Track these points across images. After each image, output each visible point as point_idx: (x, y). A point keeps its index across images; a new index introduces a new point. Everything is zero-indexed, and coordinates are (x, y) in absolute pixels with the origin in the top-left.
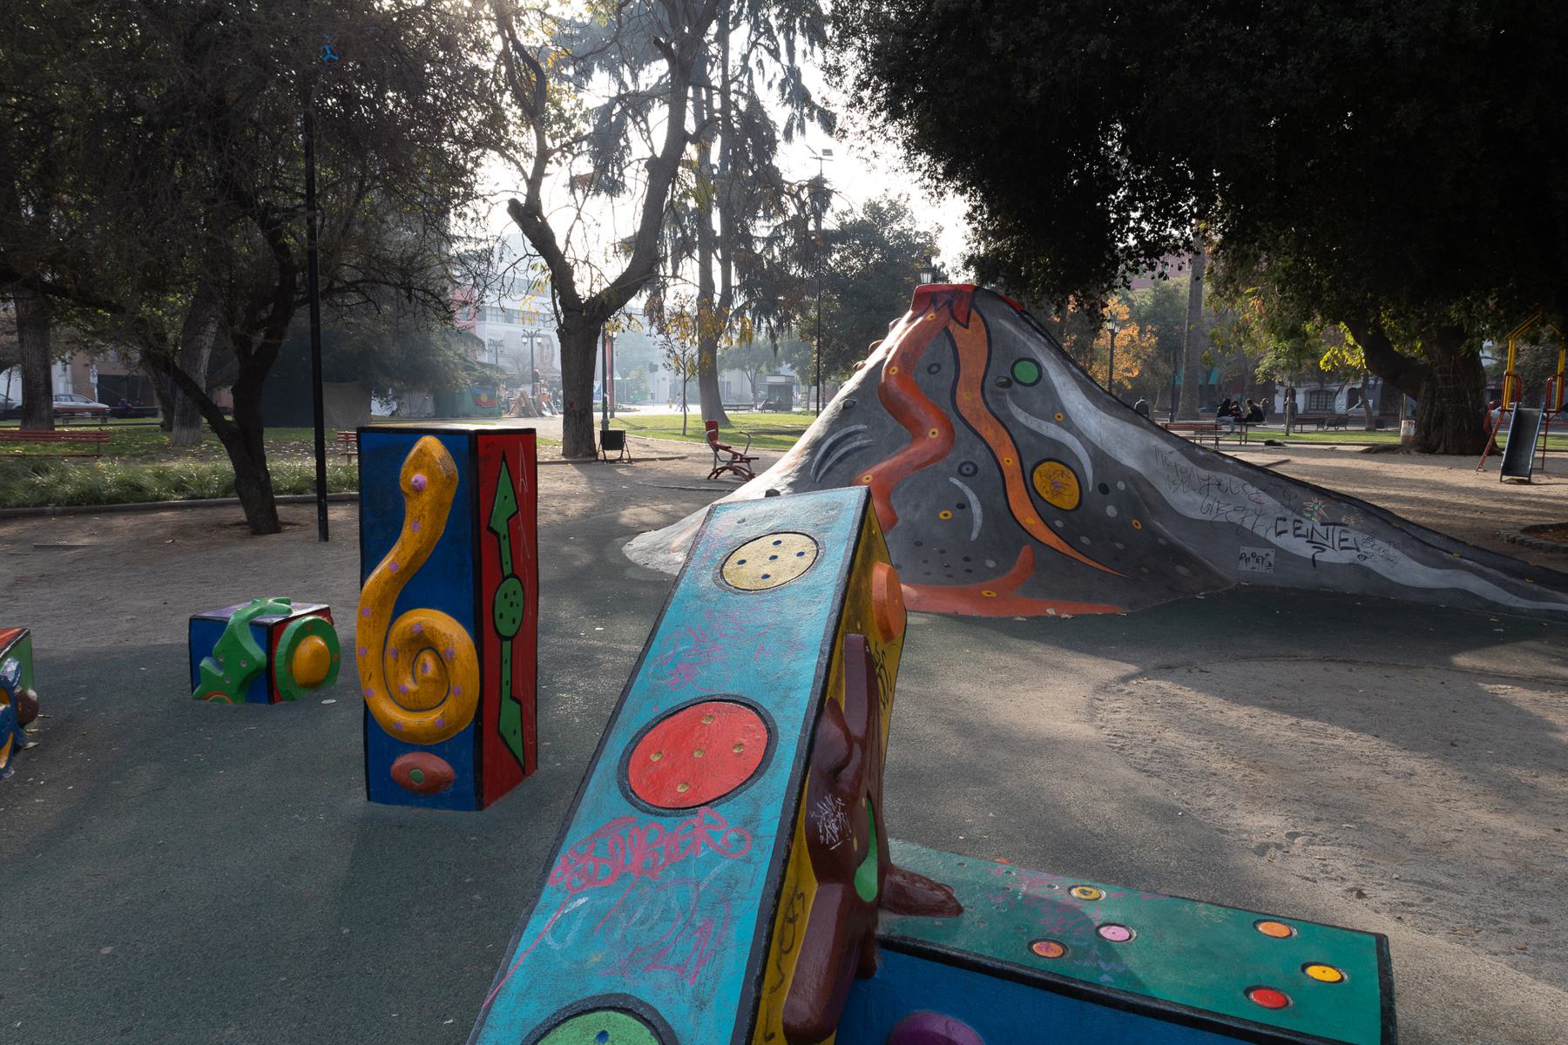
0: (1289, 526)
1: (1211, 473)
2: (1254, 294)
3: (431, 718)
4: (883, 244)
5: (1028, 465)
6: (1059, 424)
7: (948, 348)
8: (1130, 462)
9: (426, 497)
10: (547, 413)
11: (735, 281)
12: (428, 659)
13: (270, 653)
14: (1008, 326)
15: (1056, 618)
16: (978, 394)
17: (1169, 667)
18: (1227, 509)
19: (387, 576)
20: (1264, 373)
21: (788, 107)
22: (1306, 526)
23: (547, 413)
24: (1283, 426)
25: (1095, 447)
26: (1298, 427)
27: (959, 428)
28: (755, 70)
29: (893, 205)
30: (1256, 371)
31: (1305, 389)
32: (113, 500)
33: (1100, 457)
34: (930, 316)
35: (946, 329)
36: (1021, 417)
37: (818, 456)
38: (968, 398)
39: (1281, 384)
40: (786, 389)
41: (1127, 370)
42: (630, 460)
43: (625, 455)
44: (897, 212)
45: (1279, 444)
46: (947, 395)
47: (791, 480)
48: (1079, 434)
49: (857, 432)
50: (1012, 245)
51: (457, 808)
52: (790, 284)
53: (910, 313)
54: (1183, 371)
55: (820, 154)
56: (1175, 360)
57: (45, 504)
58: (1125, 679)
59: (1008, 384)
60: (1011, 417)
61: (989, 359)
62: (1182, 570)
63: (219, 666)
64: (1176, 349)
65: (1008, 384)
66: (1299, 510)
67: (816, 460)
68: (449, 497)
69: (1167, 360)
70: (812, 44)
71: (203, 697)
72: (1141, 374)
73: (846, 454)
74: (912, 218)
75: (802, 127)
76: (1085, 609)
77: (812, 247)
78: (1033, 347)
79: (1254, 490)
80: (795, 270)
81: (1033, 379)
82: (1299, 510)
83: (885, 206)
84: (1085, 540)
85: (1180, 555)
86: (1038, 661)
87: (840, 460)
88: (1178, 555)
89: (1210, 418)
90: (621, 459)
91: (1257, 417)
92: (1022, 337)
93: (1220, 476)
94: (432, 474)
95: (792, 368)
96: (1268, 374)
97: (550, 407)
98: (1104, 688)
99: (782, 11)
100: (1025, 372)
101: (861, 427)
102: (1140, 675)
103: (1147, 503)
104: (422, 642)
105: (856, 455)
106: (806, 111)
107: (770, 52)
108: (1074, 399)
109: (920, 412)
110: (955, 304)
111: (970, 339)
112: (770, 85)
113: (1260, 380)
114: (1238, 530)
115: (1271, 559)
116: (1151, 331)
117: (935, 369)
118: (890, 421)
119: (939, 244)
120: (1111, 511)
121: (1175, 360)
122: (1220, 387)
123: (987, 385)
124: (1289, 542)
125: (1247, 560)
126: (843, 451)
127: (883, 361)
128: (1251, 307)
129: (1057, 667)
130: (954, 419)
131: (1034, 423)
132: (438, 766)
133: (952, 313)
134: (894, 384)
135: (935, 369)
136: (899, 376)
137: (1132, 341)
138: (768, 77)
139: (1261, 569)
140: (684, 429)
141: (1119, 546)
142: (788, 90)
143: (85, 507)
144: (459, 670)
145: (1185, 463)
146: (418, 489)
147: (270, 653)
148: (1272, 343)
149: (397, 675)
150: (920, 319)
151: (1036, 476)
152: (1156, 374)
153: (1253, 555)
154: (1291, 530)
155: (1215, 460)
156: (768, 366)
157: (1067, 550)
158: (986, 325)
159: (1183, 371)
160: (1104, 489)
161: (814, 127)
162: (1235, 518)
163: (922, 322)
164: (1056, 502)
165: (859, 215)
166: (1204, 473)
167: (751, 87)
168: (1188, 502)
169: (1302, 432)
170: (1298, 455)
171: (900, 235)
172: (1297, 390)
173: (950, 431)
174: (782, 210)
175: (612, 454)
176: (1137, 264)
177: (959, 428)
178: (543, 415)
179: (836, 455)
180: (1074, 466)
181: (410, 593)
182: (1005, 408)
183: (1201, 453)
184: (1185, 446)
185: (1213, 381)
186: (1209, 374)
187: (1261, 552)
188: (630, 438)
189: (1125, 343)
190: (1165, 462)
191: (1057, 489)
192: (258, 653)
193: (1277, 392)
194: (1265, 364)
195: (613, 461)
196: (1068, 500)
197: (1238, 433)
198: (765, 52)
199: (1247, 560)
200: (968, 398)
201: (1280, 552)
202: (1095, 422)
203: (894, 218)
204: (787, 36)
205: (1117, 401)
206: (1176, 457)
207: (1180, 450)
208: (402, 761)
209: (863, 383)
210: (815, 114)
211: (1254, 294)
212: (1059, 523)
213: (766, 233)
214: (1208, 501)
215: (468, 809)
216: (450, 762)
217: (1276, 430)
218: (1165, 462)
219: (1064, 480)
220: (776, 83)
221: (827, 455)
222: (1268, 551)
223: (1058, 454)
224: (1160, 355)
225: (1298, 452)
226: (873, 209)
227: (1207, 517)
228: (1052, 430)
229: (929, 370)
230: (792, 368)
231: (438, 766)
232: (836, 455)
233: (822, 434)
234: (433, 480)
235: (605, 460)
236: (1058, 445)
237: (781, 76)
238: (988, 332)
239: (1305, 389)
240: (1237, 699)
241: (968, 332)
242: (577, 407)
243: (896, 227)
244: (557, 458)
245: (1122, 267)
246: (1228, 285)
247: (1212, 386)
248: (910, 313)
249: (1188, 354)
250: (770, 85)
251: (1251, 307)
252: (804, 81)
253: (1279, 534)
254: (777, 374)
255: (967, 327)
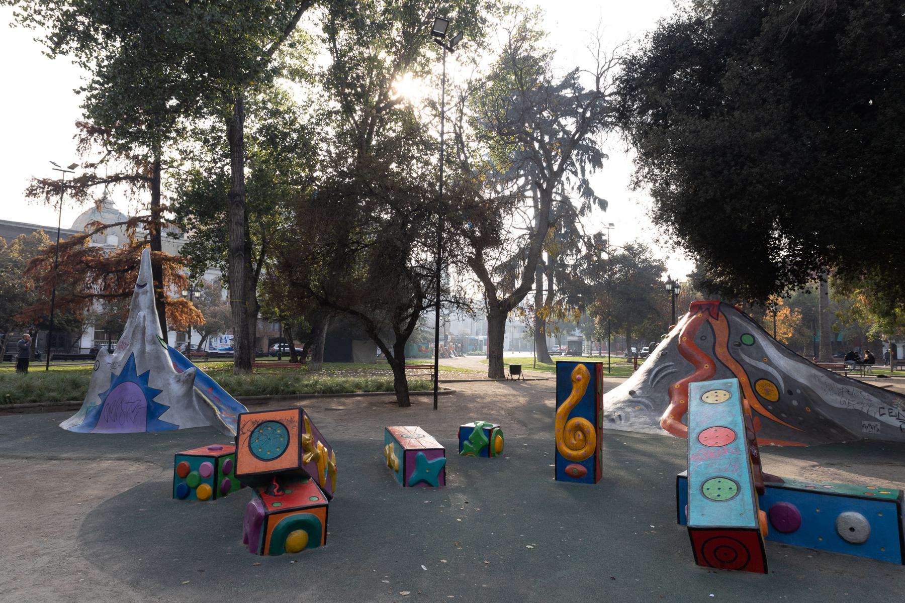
0: (886, 411)
1: (844, 386)
2: (859, 293)
3: (581, 452)
4: (635, 266)
5: (753, 381)
6: (765, 363)
7: (710, 330)
8: (802, 380)
9: (581, 382)
10: (453, 356)
11: (555, 287)
12: (580, 433)
13: (490, 440)
14: (738, 319)
15: (776, 447)
16: (726, 349)
17: (832, 464)
18: (853, 403)
19: (568, 406)
20: (872, 336)
21: (583, 198)
22: (895, 412)
23: (453, 356)
24: (889, 367)
25: (784, 373)
26: (899, 368)
27: (718, 364)
28: (565, 182)
29: (640, 245)
30: (868, 334)
31: (902, 344)
32: (337, 392)
33: (787, 378)
34: (699, 315)
35: (708, 321)
36: (747, 359)
37: (652, 376)
38: (721, 351)
39: (886, 341)
40: (579, 343)
41: (785, 333)
42: (524, 380)
43: (521, 378)
44: (643, 250)
45: (886, 377)
46: (711, 350)
47: (640, 386)
48: (776, 368)
49: (670, 366)
50: (729, 279)
51: (587, 483)
52: (587, 290)
53: (689, 313)
54: (820, 334)
55: (608, 226)
56: (814, 327)
57: (314, 393)
58: (814, 466)
59: (739, 345)
60: (743, 360)
61: (729, 334)
62: (833, 431)
63: (471, 443)
64: (815, 320)
65: (739, 345)
66: (891, 404)
67: (197, 408)
68: (588, 383)
69: (809, 328)
70: (594, 167)
71: (464, 454)
72: (793, 335)
73: (665, 375)
74: (651, 252)
75: (589, 207)
76: (789, 444)
77: (597, 268)
78: (750, 329)
79: (867, 394)
80: (587, 281)
81: (751, 343)
82: (891, 404)
83: (636, 246)
84: (784, 415)
85: (831, 424)
86: (773, 460)
87: (662, 378)
88: (831, 424)
89: (840, 361)
90: (519, 379)
91: (871, 361)
92: (744, 324)
93: (848, 387)
94: (583, 375)
95: (582, 332)
96: (877, 335)
97: (454, 353)
98: (805, 468)
99: (578, 152)
100: (747, 340)
101: (671, 363)
102: (820, 465)
103: (812, 400)
104: (579, 428)
105: (670, 376)
106: (592, 200)
107: (573, 173)
108: (772, 352)
109: (699, 358)
110: (711, 309)
111: (719, 325)
112: (573, 188)
113: (870, 340)
114: (860, 413)
115: (879, 427)
116: (798, 311)
117: (704, 338)
118: (685, 362)
119: (667, 266)
120: (795, 403)
121: (814, 327)
122: (845, 343)
123: (729, 345)
124: (886, 419)
125: (866, 427)
126: (663, 374)
127: (678, 334)
128: (859, 299)
129: (782, 462)
130: (715, 360)
131: (753, 362)
132: (581, 468)
133: (710, 314)
134: (685, 345)
135: (704, 338)
136: (687, 341)
137: (786, 316)
138: (572, 184)
139: (874, 432)
140: (535, 365)
141: (801, 419)
142: (582, 190)
143: (328, 394)
144: (591, 436)
145: (830, 381)
146: (579, 380)
147: (490, 440)
148: (876, 318)
149: (570, 438)
150: (694, 316)
151: (757, 386)
152: (803, 336)
153: (869, 425)
154: (887, 414)
155: (845, 380)
156: (567, 331)
157: (775, 419)
158: (727, 319)
159: (820, 334)
160: (790, 392)
161: (595, 207)
162: (858, 407)
163: (695, 319)
164: (767, 398)
165: (620, 252)
166: (840, 386)
167: (563, 190)
168: (834, 399)
169: (902, 370)
170: (897, 383)
171: (644, 261)
172: (897, 344)
173: (714, 366)
174: (579, 251)
175: (516, 377)
176: (793, 286)
177: (718, 364)
178: (451, 357)
179: (661, 376)
180: (775, 382)
181: (573, 412)
182: (739, 355)
183: (838, 377)
184: (831, 375)
185: (840, 339)
186: (837, 335)
187: (873, 424)
188: (523, 371)
189: (782, 318)
190: (820, 381)
191: (768, 392)
192: (486, 439)
193: (883, 346)
194: (873, 330)
195: (515, 380)
196: (774, 397)
197: (858, 370)
198: (570, 173)
199: (866, 427)
200: (721, 351)
201: (882, 423)
202: (783, 362)
203: (640, 252)
204: (581, 164)
205: (790, 349)
206: (825, 378)
207: (827, 375)
208: (568, 468)
209: (670, 344)
210: (597, 200)
211: (859, 293)
212: (770, 407)
213: (572, 262)
214: (843, 399)
215: (591, 483)
216: (585, 467)
217: (885, 369)
218: (820, 381)
219: (770, 388)
220: (576, 188)
221: (656, 375)
222: (877, 423)
223: (766, 376)
224: (804, 324)
225: (898, 382)
226: (629, 248)
227: (844, 407)
228: (762, 366)
229: (701, 338)
230: (582, 332)
231: (581, 468)
232: (661, 376)
233: (652, 367)
234: (583, 377)
235: (512, 380)
236: (766, 373)
237: (578, 183)
238: (728, 322)
239: (902, 344)
240: (864, 475)
241: (718, 322)
242: (496, 353)
243: (643, 257)
244: (487, 379)
245: (786, 288)
246: (844, 290)
247: (840, 343)
248: (689, 313)
249: (822, 324)
250: (573, 188)
251: (859, 299)
252: (591, 186)
253: (881, 415)
254: (573, 335)
255: (717, 320)
